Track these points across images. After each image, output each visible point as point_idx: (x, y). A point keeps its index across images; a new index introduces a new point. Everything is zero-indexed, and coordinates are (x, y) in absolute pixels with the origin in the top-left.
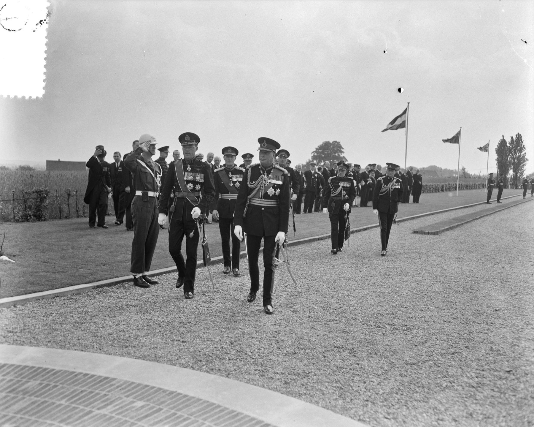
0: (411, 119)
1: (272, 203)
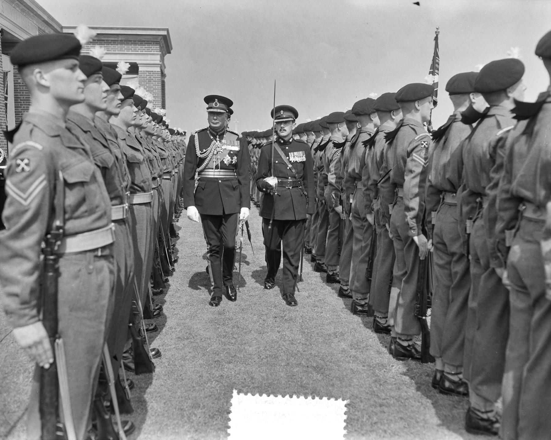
0: (416, 1)
1: (221, 173)
